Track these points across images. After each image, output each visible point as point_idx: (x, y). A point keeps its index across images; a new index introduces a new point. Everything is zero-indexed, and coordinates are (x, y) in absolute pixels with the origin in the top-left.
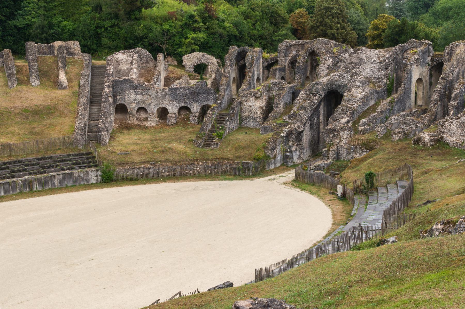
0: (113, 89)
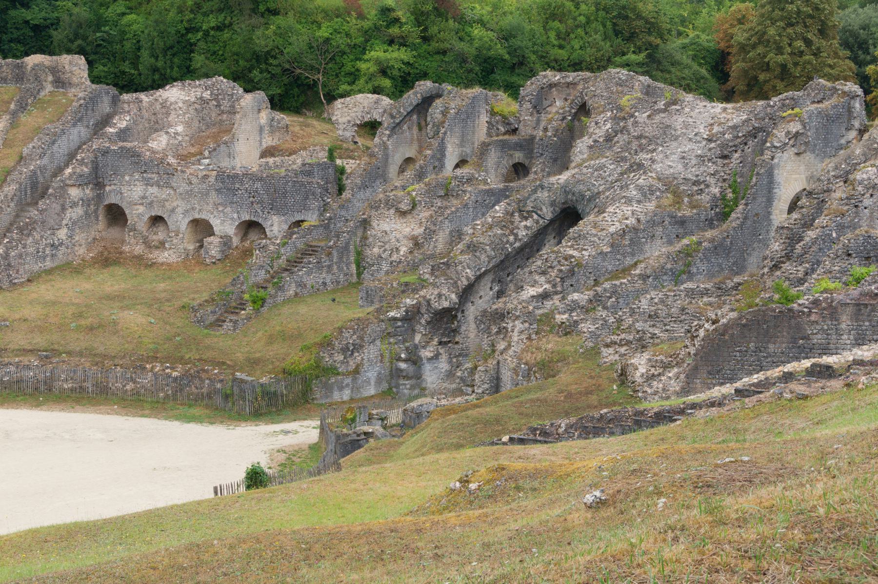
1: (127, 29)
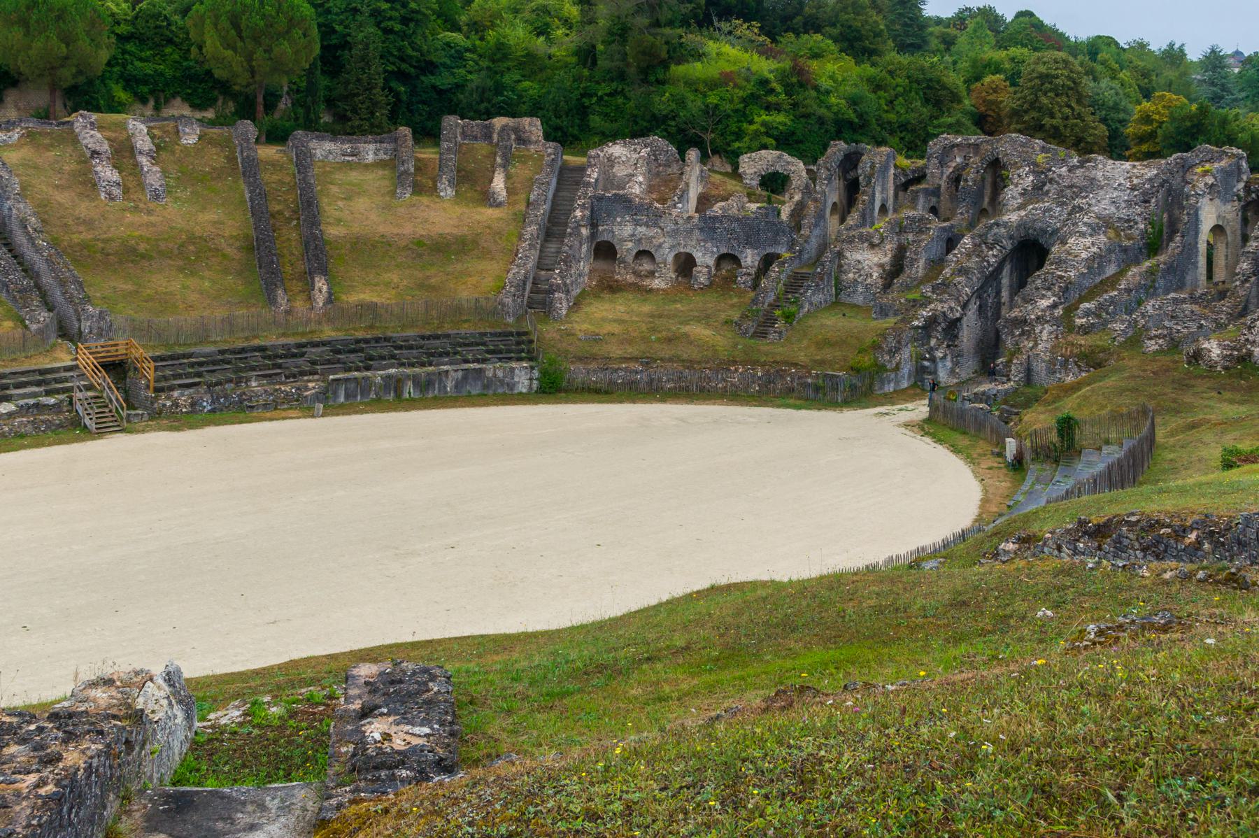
0: (592, 211)
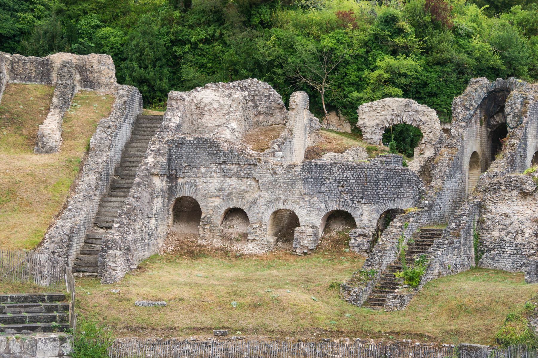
0: (170, 160)
1: (103, 42)
